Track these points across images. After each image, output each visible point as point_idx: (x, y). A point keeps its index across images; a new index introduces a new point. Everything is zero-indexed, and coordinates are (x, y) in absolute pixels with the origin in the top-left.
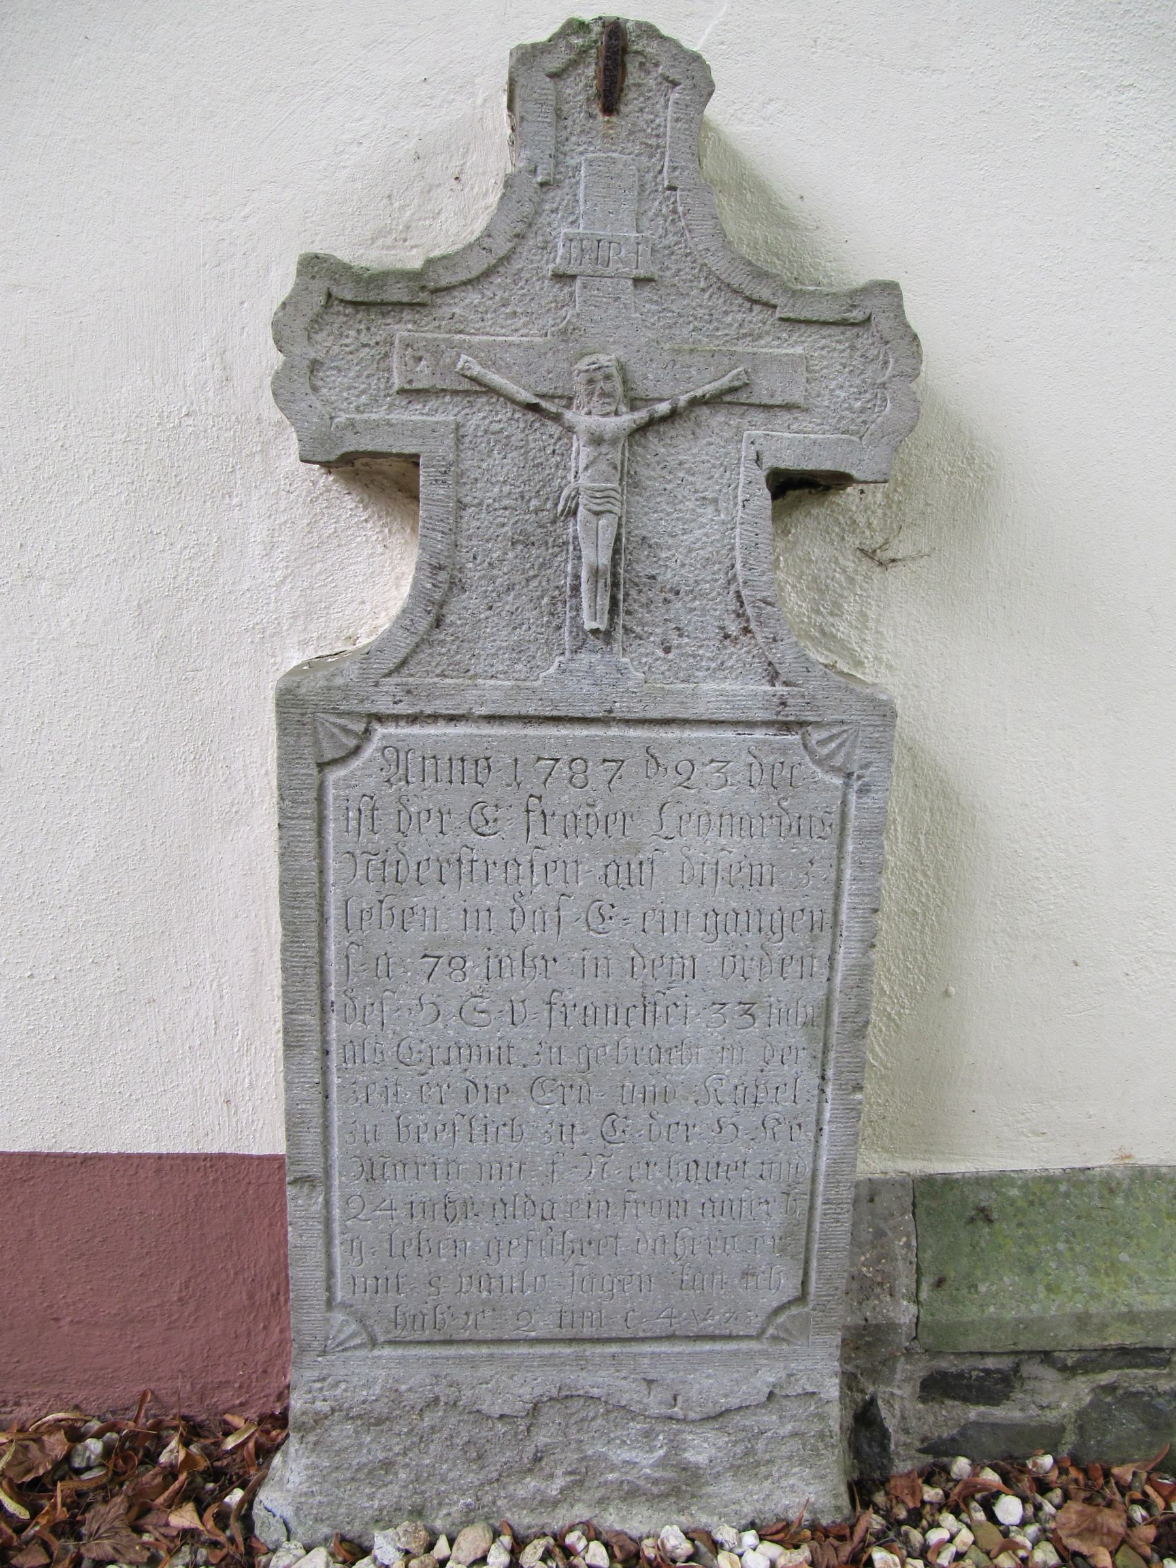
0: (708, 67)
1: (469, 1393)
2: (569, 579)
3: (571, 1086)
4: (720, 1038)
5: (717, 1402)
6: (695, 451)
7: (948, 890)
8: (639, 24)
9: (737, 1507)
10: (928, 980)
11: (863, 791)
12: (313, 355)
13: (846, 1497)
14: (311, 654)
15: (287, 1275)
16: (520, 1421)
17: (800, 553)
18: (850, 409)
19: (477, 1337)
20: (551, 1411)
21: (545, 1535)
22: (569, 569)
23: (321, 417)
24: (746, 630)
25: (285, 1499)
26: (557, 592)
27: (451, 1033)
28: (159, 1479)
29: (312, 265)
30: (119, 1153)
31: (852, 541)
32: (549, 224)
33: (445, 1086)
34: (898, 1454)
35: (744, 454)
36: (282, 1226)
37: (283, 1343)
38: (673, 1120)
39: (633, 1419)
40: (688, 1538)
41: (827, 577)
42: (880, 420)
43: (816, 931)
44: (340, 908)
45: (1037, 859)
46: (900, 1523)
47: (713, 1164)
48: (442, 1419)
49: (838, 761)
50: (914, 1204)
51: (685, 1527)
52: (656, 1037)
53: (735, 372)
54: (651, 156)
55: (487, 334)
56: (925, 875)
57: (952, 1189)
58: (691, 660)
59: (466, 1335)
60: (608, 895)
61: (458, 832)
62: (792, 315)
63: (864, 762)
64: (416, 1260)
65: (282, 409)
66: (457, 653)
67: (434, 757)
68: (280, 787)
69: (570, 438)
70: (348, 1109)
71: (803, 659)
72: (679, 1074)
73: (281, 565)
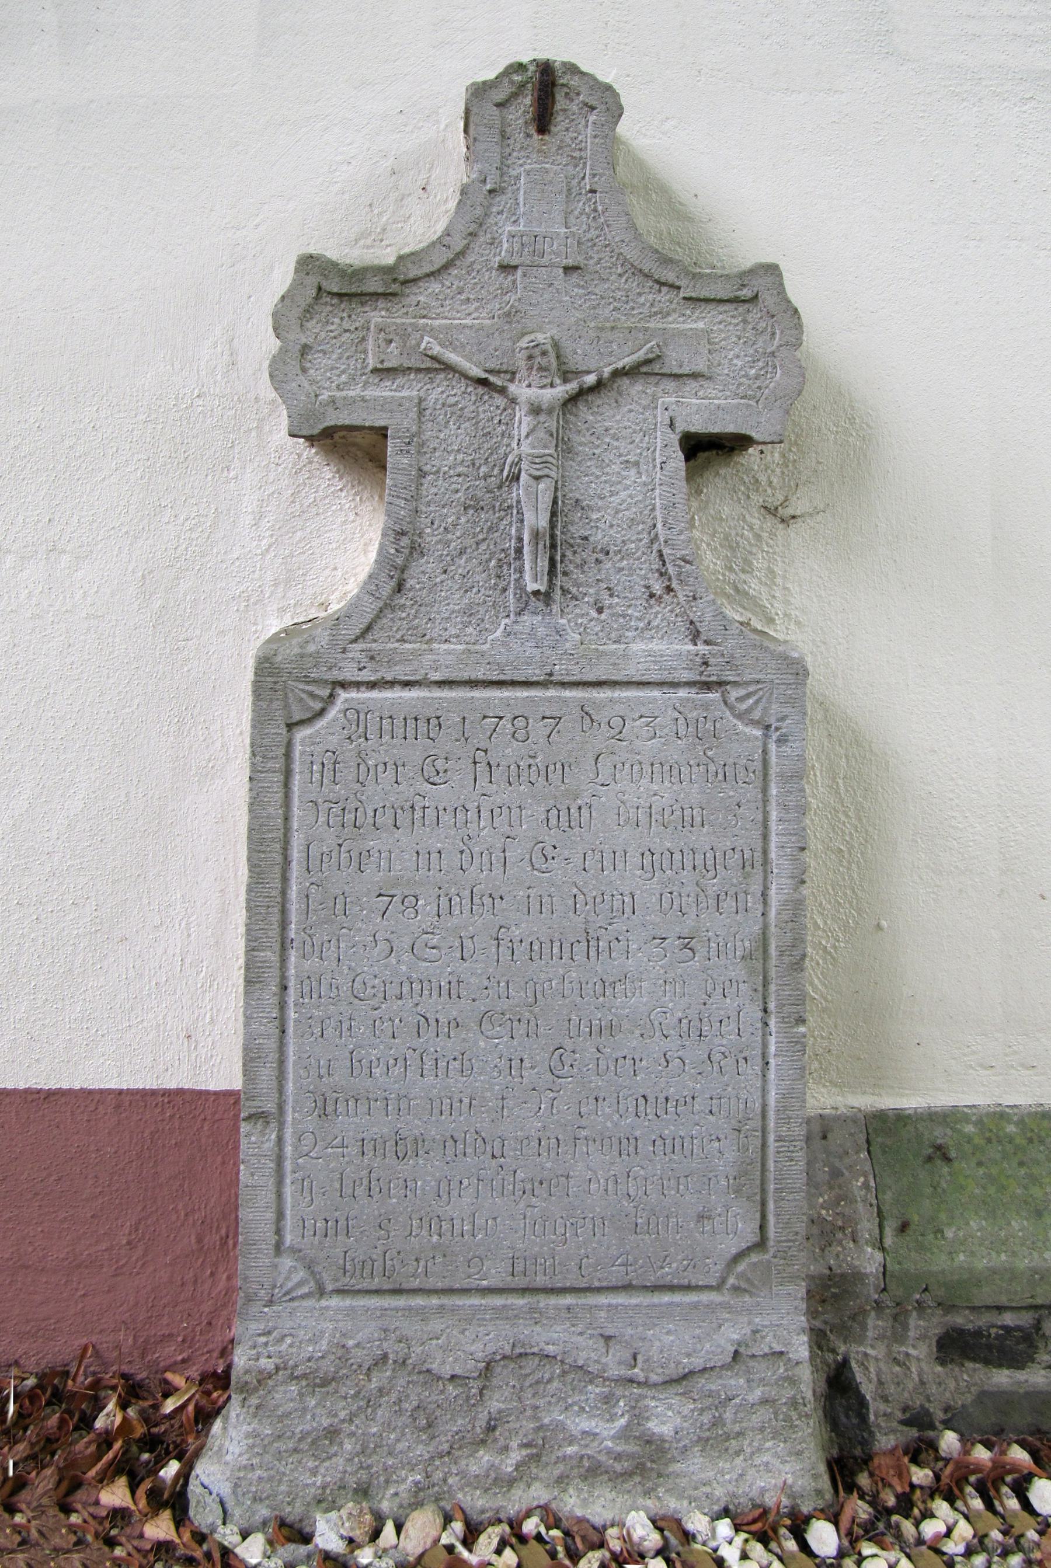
0: (618, 94)
1: (419, 1350)
2: (513, 541)
3: (519, 1020)
4: (662, 972)
5: (680, 1363)
6: (618, 418)
7: (870, 829)
8: (564, 64)
9: (707, 1489)
10: (859, 914)
11: (782, 741)
12: (304, 340)
13: (826, 1478)
14: (288, 621)
15: (237, 1217)
16: (472, 1383)
17: (712, 512)
18: (746, 376)
19: (428, 1286)
20: (505, 1372)
21: (500, 1521)
22: (513, 532)
23: (308, 395)
24: (669, 589)
25: (223, 1473)
26: (503, 555)
27: (404, 968)
28: (93, 1448)
29: (308, 264)
30: (82, 1089)
31: (757, 499)
32: (496, 224)
33: (397, 1021)
34: (879, 1426)
35: (659, 419)
36: (235, 1164)
37: (230, 1291)
38: (620, 1054)
39: (591, 1382)
40: (657, 1528)
41: (737, 534)
42: (772, 385)
43: (748, 868)
44: (303, 851)
45: (951, 799)
46: (889, 1512)
47: (662, 1100)
48: (391, 1379)
49: (756, 715)
50: (868, 1142)
51: (652, 1514)
52: (600, 971)
53: (649, 346)
54: (576, 166)
55: (446, 318)
56: (847, 816)
57: (905, 1126)
58: (621, 620)
59: (416, 1283)
60: (550, 837)
61: (411, 782)
62: (693, 295)
63: (780, 715)
64: (366, 1200)
65: (276, 389)
66: (415, 617)
67: (391, 717)
68: (252, 745)
69: (514, 409)
70: (303, 1043)
71: (720, 617)
72: (623, 1008)
73: (267, 534)
